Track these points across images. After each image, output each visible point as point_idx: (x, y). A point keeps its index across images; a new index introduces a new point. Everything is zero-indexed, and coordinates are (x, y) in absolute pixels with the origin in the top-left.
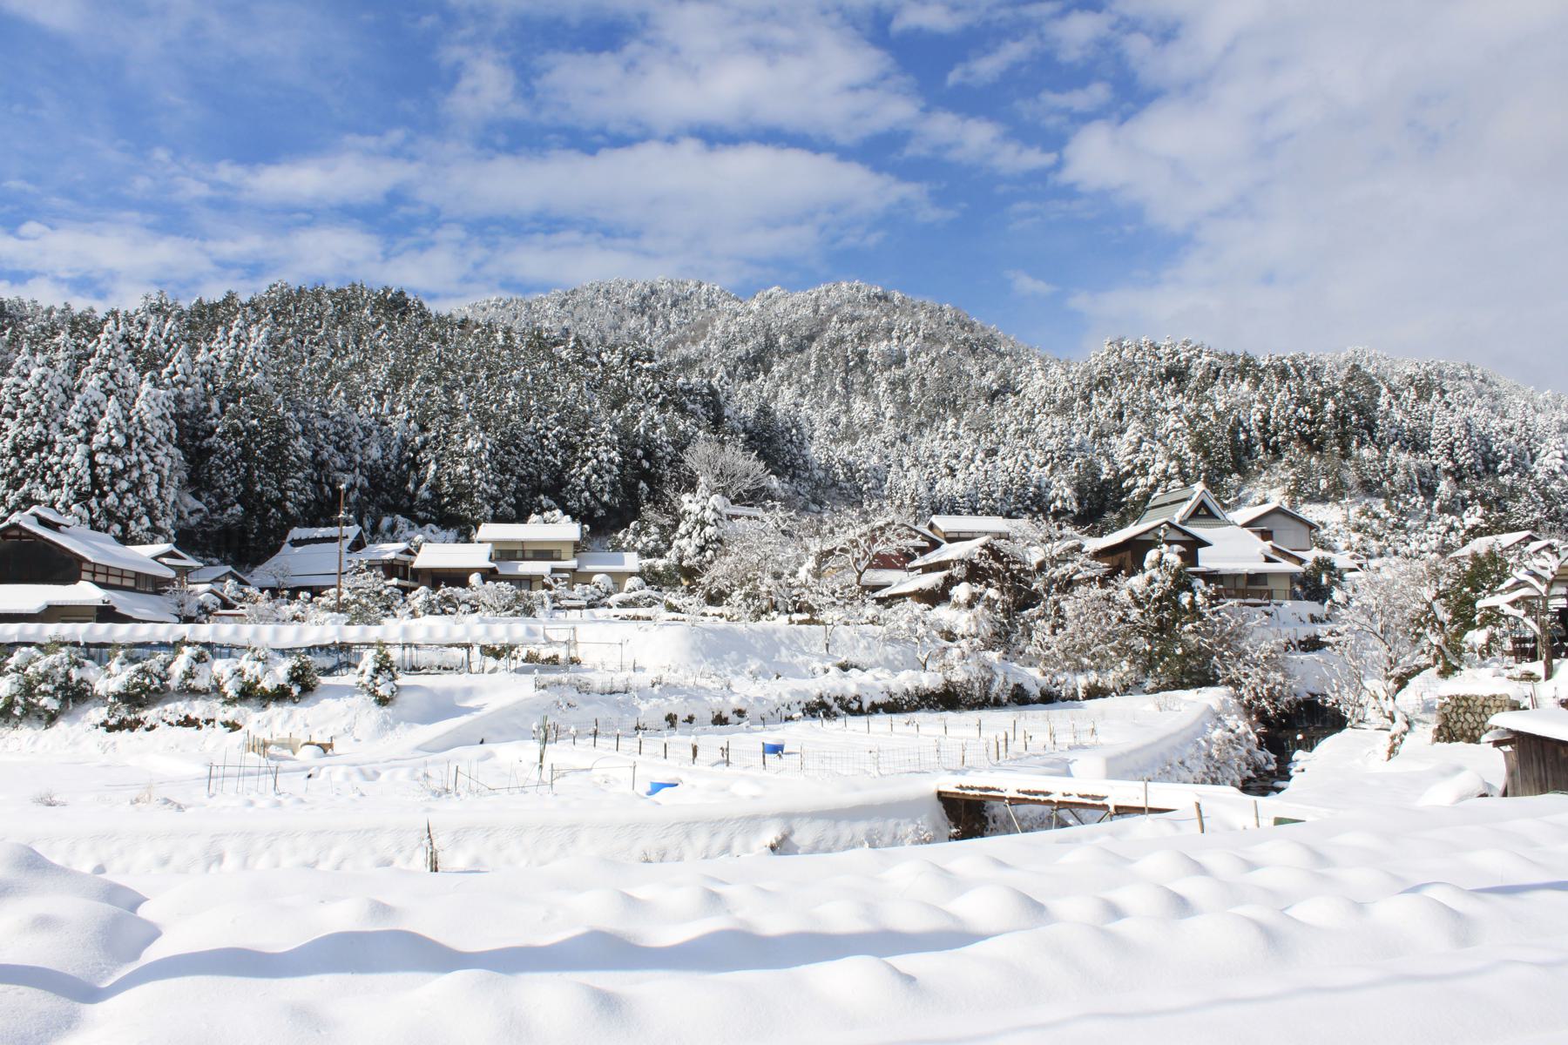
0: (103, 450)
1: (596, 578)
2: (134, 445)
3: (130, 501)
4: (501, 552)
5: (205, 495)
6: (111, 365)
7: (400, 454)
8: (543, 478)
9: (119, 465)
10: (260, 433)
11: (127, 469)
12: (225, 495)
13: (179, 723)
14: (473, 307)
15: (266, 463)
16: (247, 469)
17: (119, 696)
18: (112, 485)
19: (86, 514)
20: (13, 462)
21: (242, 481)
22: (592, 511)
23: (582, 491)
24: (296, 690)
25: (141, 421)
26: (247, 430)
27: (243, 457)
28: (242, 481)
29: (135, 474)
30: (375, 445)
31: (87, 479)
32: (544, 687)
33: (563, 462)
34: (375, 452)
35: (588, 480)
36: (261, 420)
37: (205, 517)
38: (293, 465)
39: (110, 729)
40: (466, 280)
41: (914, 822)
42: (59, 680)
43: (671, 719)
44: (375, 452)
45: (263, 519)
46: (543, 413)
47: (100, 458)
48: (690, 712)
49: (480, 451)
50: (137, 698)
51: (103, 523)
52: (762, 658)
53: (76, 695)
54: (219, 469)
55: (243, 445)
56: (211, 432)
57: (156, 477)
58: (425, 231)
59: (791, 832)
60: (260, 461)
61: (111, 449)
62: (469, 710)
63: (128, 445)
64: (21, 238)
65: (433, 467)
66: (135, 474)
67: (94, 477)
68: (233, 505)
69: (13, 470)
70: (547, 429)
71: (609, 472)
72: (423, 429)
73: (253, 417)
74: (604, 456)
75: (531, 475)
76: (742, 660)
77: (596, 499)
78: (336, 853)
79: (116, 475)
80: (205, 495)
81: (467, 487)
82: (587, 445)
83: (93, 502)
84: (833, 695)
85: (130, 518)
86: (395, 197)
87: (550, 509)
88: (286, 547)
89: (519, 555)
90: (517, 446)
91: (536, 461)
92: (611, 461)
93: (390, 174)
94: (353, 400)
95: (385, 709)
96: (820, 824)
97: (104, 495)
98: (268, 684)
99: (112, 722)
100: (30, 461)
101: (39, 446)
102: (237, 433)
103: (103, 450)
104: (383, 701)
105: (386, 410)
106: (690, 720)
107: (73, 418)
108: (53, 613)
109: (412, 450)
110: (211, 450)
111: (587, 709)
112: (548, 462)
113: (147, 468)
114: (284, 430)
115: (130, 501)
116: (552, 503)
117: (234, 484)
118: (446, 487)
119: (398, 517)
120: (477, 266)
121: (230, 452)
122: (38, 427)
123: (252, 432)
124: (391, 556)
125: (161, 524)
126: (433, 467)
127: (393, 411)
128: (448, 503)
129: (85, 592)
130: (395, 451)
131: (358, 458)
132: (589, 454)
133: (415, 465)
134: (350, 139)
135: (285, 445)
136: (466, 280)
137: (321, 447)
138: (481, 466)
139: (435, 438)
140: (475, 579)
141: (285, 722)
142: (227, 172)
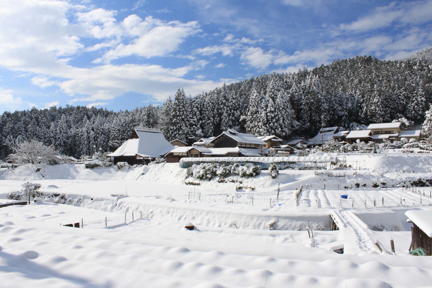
0: (269, 112)
1: (402, 139)
2: (277, 110)
3: (276, 124)
4: (375, 132)
5: (301, 121)
6: (273, 90)
7: (357, 104)
8: (400, 108)
9: (273, 115)
10: (314, 103)
11: (275, 116)
12: (306, 120)
13: (231, 182)
14: (418, 54)
15: (315, 111)
16: (310, 113)
17: (221, 175)
18: (272, 120)
19: (266, 128)
20: (251, 117)
21: (309, 116)
22: (416, 117)
23: (412, 111)
24: (254, 174)
25: (278, 104)
26: (310, 103)
27: (309, 110)
28: (309, 116)
29: (277, 117)
30: (350, 103)
31: (266, 120)
32: (318, 175)
33: (406, 103)
34: (350, 105)
35: (414, 107)
36: (314, 100)
37: (301, 127)
38: (323, 111)
39: (219, 182)
40: (421, 43)
41: (318, 223)
42: (211, 171)
43: (358, 185)
44: (350, 105)
45: (315, 126)
46: (399, 88)
47: (268, 114)
48: (365, 183)
49: (378, 102)
50: (226, 175)
51: (270, 130)
52: (410, 166)
53: (214, 174)
54: (304, 114)
55: (309, 107)
56: (301, 104)
57: (282, 118)
58: (406, 31)
59: (278, 221)
60: (314, 111)
61: (271, 112)
62: (297, 180)
63: (275, 111)
64: (295, 55)
65: (365, 108)
66: (277, 117)
67: (267, 118)
68: (307, 123)
69: (251, 119)
70: (401, 93)
71: (422, 104)
72: (363, 97)
73: (312, 99)
74: (419, 99)
75: (396, 107)
76: (402, 166)
77: (417, 113)
78: (186, 214)
79: (272, 118)
80: (301, 121)
81: (374, 113)
82: (414, 96)
83: (267, 125)
84: (425, 179)
85: (276, 128)
86: (394, 23)
87: (401, 117)
88: (319, 133)
89: (380, 133)
90: (391, 99)
91: (397, 103)
92: (422, 101)
93: (391, 16)
94: (344, 90)
95: (274, 180)
96: (287, 220)
97: (270, 123)
98: (248, 173)
99: (220, 181)
100: (254, 116)
101: (256, 113)
102: (308, 104)
103: (269, 112)
104: (274, 178)
105: (353, 93)
106: (365, 185)
107: (263, 105)
108: (229, 155)
109: (360, 103)
110: (302, 109)
111: (330, 181)
112: (401, 103)
113: (280, 116)
114: (321, 102)
115: (276, 124)
116: (402, 115)
117: (307, 117)
118: (369, 113)
119: (354, 123)
120: (425, 39)
121: (306, 109)
122: (255, 108)
123: (312, 103)
124: (343, 135)
125: (284, 129)
126: (365, 108)
127: (355, 93)
128: (369, 118)
129: (236, 150)
130: (355, 104)
131: (345, 107)
132: (414, 99)
133: (361, 108)
134: (378, 8)
135: (320, 106)
136: (421, 43)
137: (334, 105)
138: (378, 106)
139: (366, 99)
140: (358, 141)
141: (251, 182)
142: (342, 26)
